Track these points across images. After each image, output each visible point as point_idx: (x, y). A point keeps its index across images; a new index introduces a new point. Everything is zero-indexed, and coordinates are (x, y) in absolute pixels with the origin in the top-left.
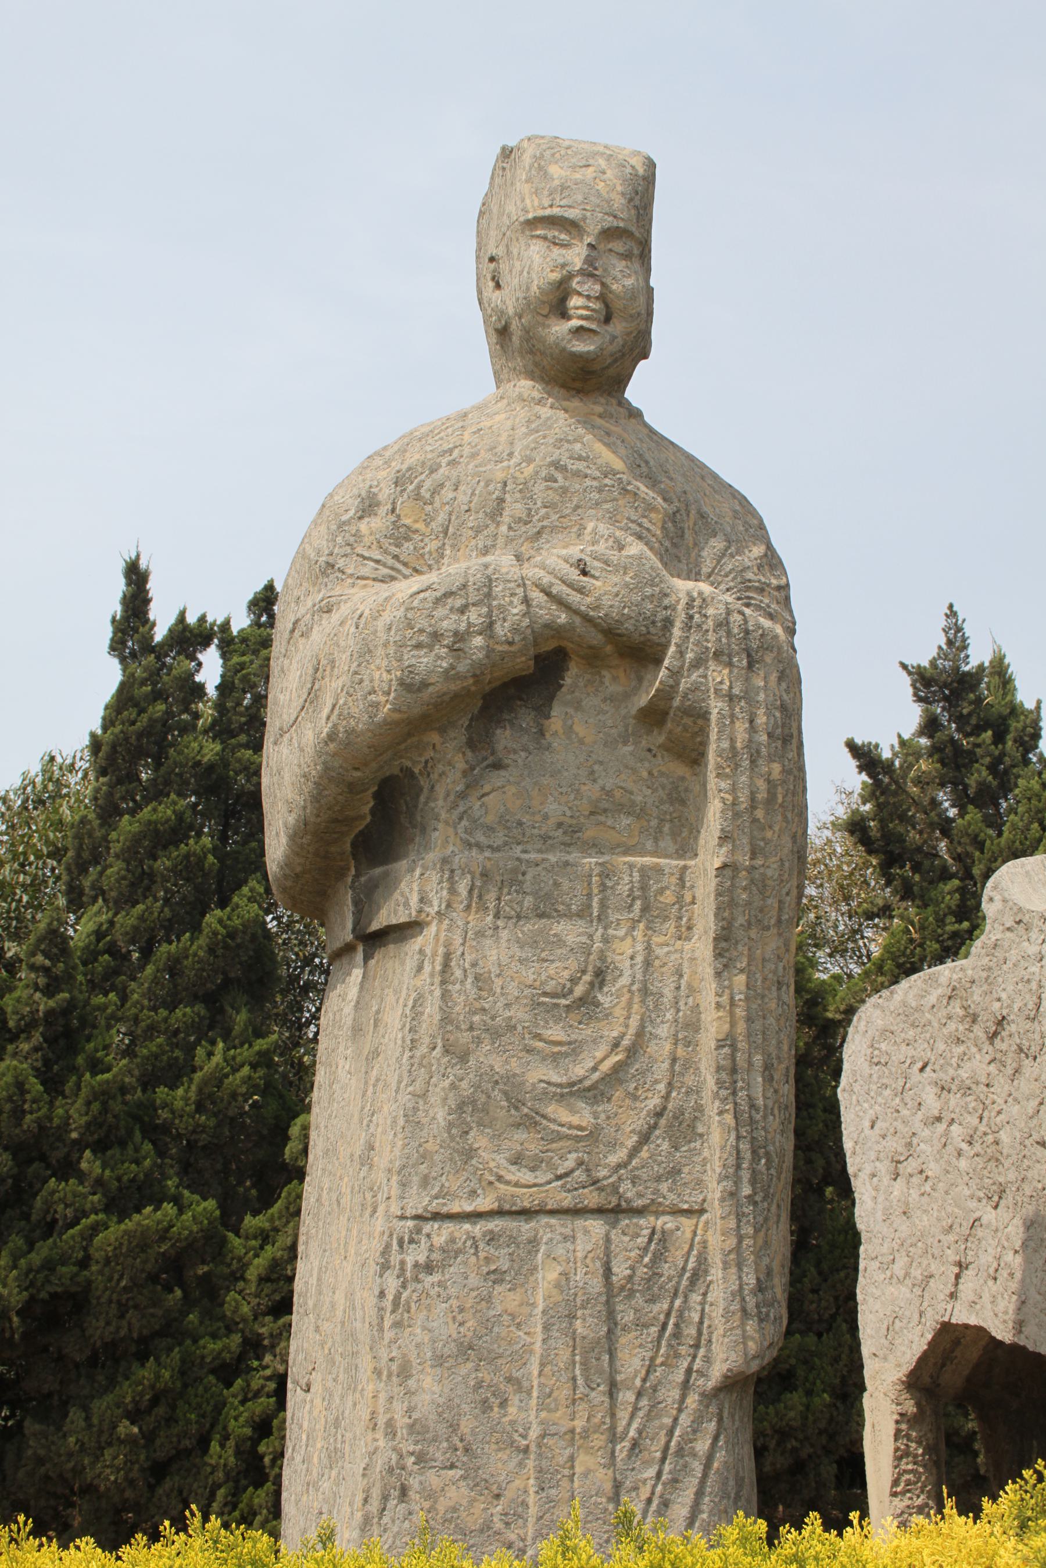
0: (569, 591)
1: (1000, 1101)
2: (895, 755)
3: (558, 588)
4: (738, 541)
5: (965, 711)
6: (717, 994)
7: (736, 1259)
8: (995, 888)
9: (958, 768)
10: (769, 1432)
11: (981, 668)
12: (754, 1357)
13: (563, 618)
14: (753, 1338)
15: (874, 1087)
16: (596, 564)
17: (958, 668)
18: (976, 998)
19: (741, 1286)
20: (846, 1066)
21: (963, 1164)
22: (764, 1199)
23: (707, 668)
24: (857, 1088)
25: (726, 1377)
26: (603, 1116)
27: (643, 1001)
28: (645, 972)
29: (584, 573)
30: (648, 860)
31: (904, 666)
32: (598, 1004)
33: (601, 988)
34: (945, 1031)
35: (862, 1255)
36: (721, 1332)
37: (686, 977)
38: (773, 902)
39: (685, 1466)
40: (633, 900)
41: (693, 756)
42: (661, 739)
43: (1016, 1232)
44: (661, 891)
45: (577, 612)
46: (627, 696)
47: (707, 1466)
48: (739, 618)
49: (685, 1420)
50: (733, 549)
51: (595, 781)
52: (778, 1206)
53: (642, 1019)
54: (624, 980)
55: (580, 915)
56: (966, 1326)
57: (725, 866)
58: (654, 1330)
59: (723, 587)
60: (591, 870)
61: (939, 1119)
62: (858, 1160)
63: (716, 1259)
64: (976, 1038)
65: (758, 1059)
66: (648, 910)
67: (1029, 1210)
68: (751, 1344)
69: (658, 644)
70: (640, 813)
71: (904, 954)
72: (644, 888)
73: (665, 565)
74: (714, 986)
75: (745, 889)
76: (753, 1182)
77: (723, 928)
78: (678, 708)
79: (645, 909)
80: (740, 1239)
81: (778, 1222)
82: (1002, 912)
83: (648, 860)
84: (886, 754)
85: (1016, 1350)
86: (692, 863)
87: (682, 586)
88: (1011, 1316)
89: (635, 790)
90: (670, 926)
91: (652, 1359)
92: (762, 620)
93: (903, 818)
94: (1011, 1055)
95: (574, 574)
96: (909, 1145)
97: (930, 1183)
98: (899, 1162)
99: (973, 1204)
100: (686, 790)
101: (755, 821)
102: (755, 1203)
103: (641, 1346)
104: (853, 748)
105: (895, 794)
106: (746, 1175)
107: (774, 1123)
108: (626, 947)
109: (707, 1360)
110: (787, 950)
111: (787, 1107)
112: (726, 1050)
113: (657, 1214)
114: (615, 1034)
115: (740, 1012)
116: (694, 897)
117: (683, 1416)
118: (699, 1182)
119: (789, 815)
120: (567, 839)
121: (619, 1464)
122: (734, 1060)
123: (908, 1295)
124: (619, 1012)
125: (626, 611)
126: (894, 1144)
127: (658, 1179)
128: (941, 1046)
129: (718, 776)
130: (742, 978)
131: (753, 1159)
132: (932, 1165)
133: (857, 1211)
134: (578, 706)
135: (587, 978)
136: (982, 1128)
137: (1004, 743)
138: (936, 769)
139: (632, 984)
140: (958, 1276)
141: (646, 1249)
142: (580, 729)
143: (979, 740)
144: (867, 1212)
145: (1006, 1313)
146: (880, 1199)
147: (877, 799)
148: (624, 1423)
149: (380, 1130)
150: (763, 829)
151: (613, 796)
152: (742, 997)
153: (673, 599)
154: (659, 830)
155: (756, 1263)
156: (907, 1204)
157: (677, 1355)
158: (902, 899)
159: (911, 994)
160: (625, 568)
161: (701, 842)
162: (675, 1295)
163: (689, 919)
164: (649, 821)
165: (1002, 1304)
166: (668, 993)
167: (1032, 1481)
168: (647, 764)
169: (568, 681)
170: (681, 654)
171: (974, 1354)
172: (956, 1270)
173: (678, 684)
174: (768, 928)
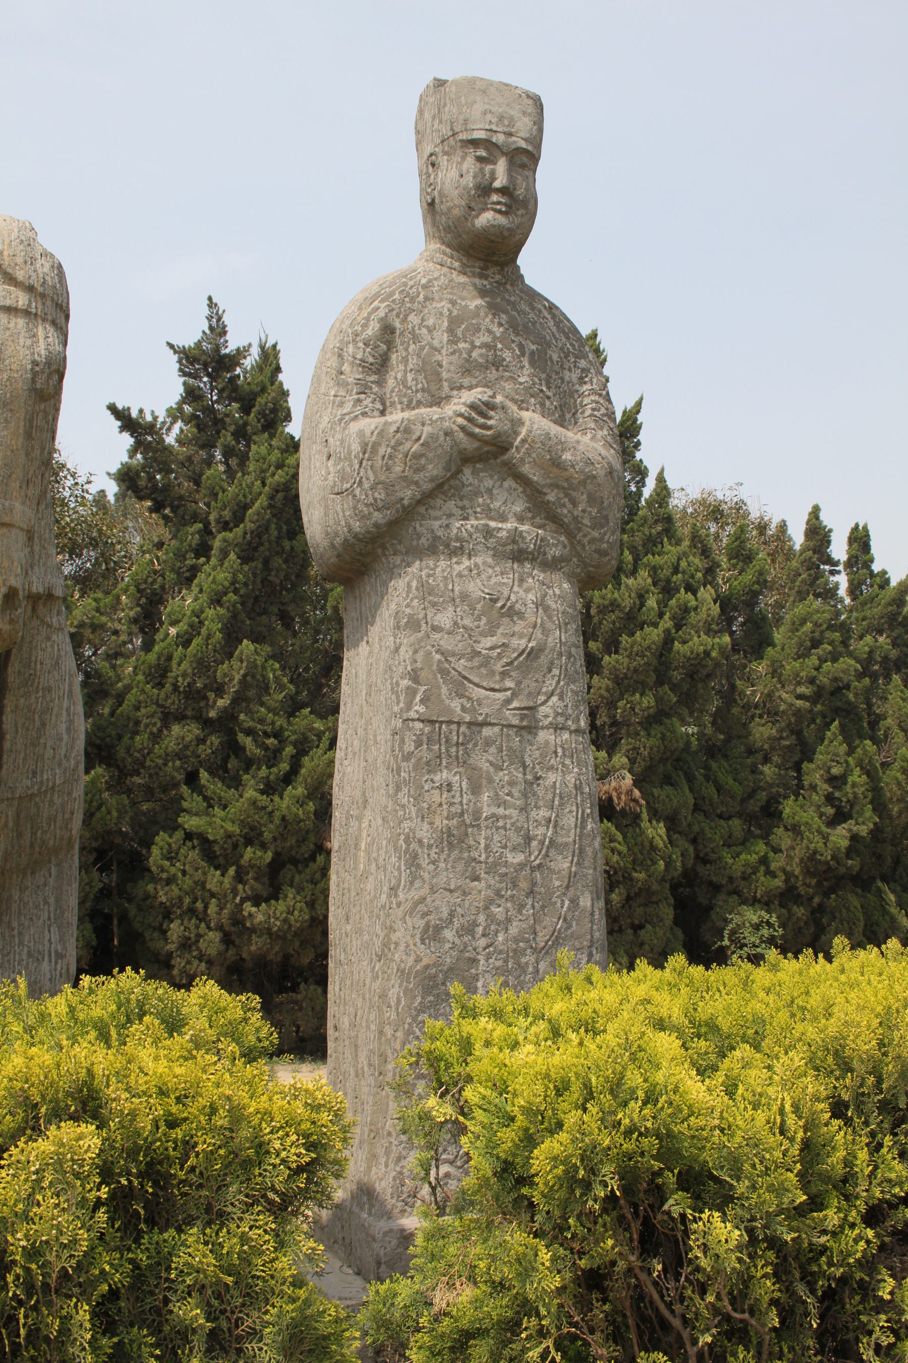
31: (171, 346)
71: (146, 582)
138: (192, 433)
149: (382, 852)
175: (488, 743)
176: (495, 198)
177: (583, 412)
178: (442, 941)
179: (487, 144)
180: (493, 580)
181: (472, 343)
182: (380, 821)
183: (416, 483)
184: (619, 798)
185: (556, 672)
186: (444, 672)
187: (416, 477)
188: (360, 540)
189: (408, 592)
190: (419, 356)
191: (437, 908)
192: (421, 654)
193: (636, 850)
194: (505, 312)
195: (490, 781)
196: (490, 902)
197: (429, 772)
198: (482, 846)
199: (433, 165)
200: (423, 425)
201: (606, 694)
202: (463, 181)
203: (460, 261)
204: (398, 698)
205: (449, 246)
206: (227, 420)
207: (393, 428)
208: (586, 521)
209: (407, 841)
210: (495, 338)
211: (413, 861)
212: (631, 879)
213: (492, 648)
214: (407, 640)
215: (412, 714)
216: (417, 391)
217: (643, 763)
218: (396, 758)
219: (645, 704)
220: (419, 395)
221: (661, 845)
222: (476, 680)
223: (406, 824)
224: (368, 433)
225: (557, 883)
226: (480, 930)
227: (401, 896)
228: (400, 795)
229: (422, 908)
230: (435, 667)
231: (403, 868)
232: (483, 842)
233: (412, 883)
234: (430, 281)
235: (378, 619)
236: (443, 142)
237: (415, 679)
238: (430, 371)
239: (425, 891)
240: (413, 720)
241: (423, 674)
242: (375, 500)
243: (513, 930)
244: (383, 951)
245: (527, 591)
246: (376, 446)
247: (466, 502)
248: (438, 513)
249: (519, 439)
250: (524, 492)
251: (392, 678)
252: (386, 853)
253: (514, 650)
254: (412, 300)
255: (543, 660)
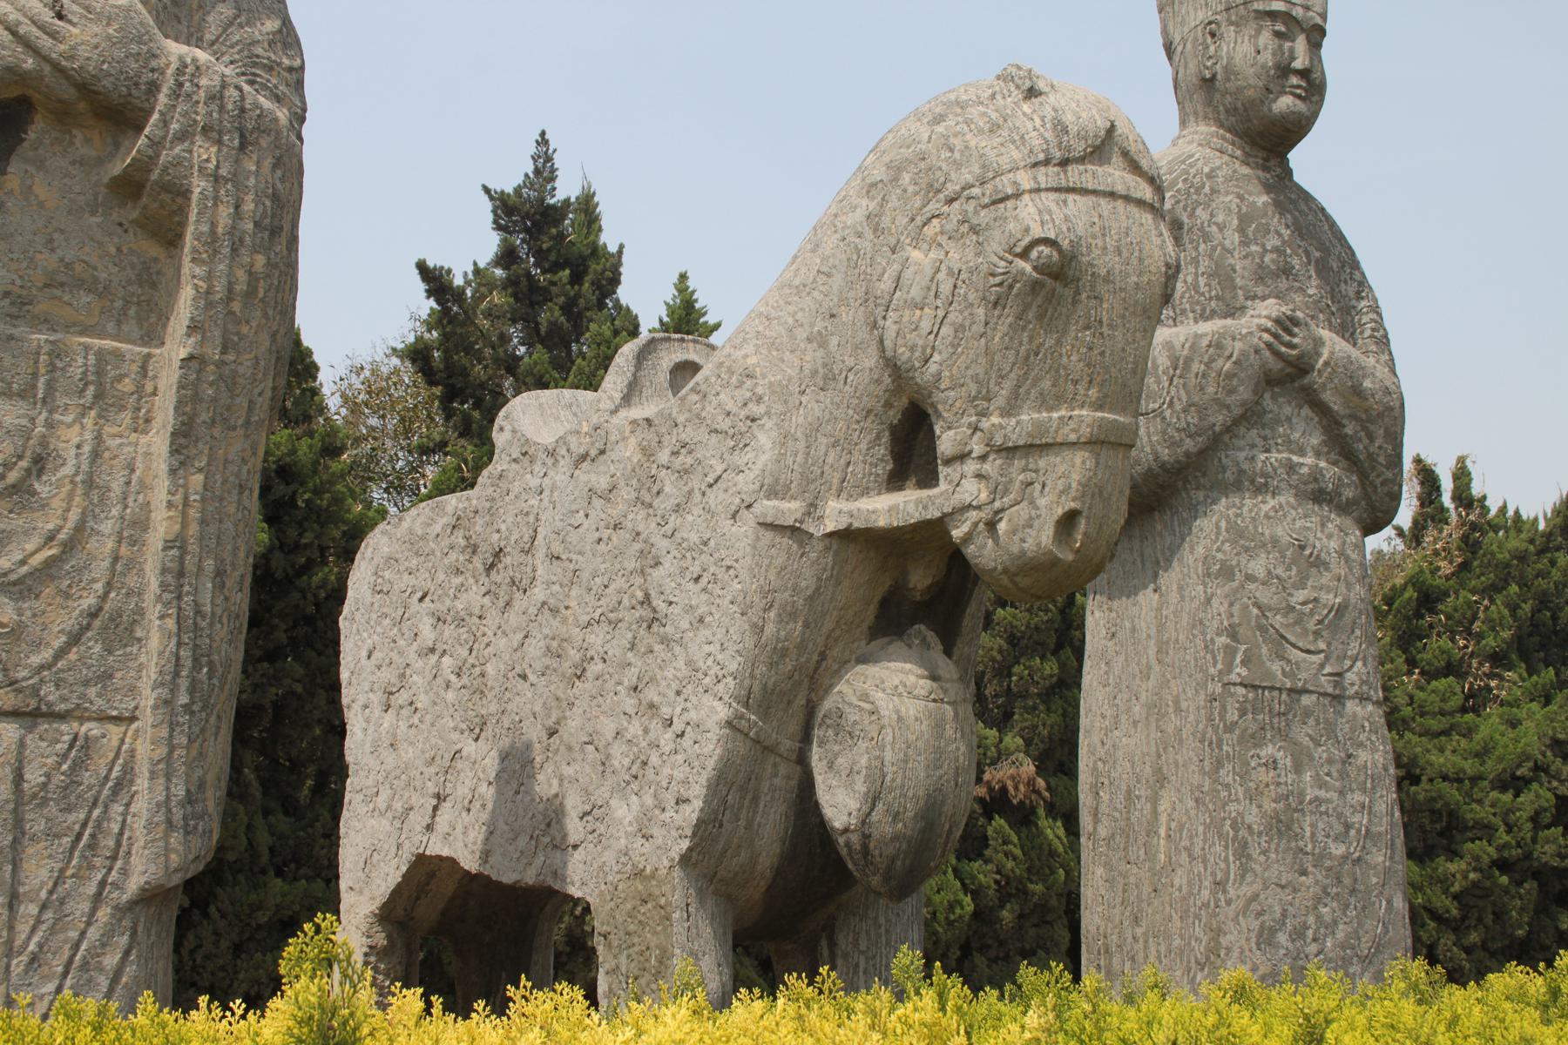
0: (39, 33)
1: (490, 633)
2: (468, 283)
3: (26, 28)
4: (250, 11)
5: (545, 246)
6: (169, 493)
7: (164, 769)
8: (506, 417)
9: (532, 305)
10: (264, 980)
11: (567, 202)
12: (176, 870)
13: (29, 63)
14: (177, 851)
15: (374, 616)
16: (75, 8)
17: (543, 200)
18: (478, 528)
19: (168, 797)
20: (350, 593)
21: (450, 696)
22: (203, 709)
23: (193, 143)
24: (358, 616)
25: (143, 890)
26: (28, 613)
27: (86, 494)
28: (92, 463)
29: (60, 16)
30: (108, 344)
31: (487, 190)
32: (34, 493)
33: (39, 476)
34: (446, 561)
35: (348, 788)
36: (142, 843)
37: (138, 473)
38: (242, 401)
39: (89, 981)
40: (86, 384)
41: (171, 239)
42: (135, 214)
43: (491, 764)
44: (119, 379)
45: (46, 59)
46: (100, 162)
47: (115, 980)
48: (236, 93)
49: (93, 933)
50: (243, 19)
51: (53, 250)
52: (219, 717)
53: (83, 513)
54: (67, 470)
55: (22, 395)
56: (439, 857)
57: (191, 358)
58: (67, 840)
59: (226, 58)
60: (40, 347)
61: (432, 650)
62: (353, 691)
63: (143, 769)
64: (475, 569)
65: (209, 564)
66: (102, 396)
67: (506, 742)
68: (173, 856)
69: (141, 109)
70: (104, 292)
72: (100, 373)
73: (161, 24)
74: (167, 483)
75: (211, 384)
76: (192, 691)
77: (183, 423)
78: (156, 182)
79: (98, 396)
80: (172, 749)
81: (216, 735)
82: (510, 443)
83: (108, 344)
84: (458, 281)
85: (478, 877)
86: (158, 351)
87: (175, 50)
88: (479, 846)
89: (100, 266)
90: (126, 417)
91: (62, 871)
92: (262, 99)
93: (468, 350)
94: (504, 587)
95: (47, 16)
96: (403, 675)
97: (418, 715)
98: (391, 693)
99: (455, 736)
100: (159, 272)
101: (230, 313)
102: (192, 713)
103: (50, 856)
104: (423, 269)
105: (463, 324)
106: (184, 683)
107: (221, 631)
108: (73, 435)
109: (125, 872)
110: (254, 454)
111: (238, 616)
112: (174, 552)
113: (82, 720)
114: (51, 526)
115: (193, 513)
116: (156, 388)
117: (92, 930)
118: (132, 689)
119: (270, 312)
120: (14, 310)
121: (14, 979)
122: (182, 563)
123: (388, 828)
124: (57, 504)
125: (105, 66)
126: (389, 675)
127: (86, 683)
128: (441, 576)
129: (193, 260)
130: (200, 478)
131: (194, 668)
132: (422, 697)
133: (348, 743)
134: (41, 165)
135: (24, 464)
136: (471, 660)
137: (581, 285)
139: (76, 475)
140: (435, 808)
141: (65, 756)
142: (41, 191)
143: (556, 278)
144: (356, 746)
145: (475, 843)
146: (370, 731)
147: (444, 327)
148: (23, 936)
150: (239, 323)
151: (73, 269)
152: (197, 497)
153: (163, 60)
154: (124, 312)
155: (187, 774)
156: (395, 736)
157: (91, 867)
158: (461, 435)
159: (419, 521)
160: (109, 19)
161: (170, 330)
162: (95, 804)
163: (148, 411)
164: (112, 301)
165: (472, 835)
166: (116, 488)
167: (311, 934)
168: (116, 240)
169: (32, 135)
170: (165, 123)
171: (449, 887)
172: (434, 802)
173: (159, 156)
174: (234, 428)
175: (1307, 713)
176: (1294, 80)
177: (1362, 333)
178: (1277, 946)
179: (1286, 17)
180: (1298, 524)
181: (1263, 246)
182: (1191, 803)
183: (1228, 407)
184: (1016, 788)
185: (1358, 632)
186: (1262, 629)
187: (1228, 400)
188: (1166, 471)
189: (1218, 534)
190: (1210, 257)
191: (1270, 907)
192: (1237, 607)
193: (1033, 854)
194: (1290, 212)
195: (1311, 758)
196: (1318, 900)
197: (1255, 746)
198: (1308, 834)
199: (1213, 35)
200: (1234, 339)
201: (999, 658)
202: (1261, 59)
203: (1243, 149)
204: (1214, 658)
205: (1229, 131)
206: (554, 289)
207: (1205, 342)
208: (1381, 460)
209: (1234, 826)
210: (1284, 242)
211: (1242, 851)
212: (1026, 893)
213: (1304, 603)
214: (1220, 590)
215: (1234, 678)
216: (1211, 299)
217: (1041, 746)
218: (1215, 729)
219: (1048, 671)
220: (1213, 304)
221: (1061, 849)
222: (1292, 639)
223: (1232, 807)
224: (1178, 346)
225: (1374, 880)
226: (1310, 933)
227: (1232, 893)
228: (1222, 772)
229: (1255, 906)
230: (1253, 623)
231: (1231, 858)
232: (1308, 829)
233: (1243, 877)
234: (1212, 170)
235: (1175, 563)
236: (1227, 10)
237: (1234, 636)
238: (1221, 274)
239: (1257, 887)
240: (1235, 684)
241: (1242, 631)
242: (1188, 424)
243: (1340, 935)
244: (1208, 958)
245: (1329, 537)
246: (1188, 361)
247: (1268, 432)
248: (1242, 443)
249: (1321, 362)
250: (1320, 423)
251: (1204, 633)
252: (1205, 841)
253: (1325, 606)
254: (1198, 192)
255: (1348, 619)
